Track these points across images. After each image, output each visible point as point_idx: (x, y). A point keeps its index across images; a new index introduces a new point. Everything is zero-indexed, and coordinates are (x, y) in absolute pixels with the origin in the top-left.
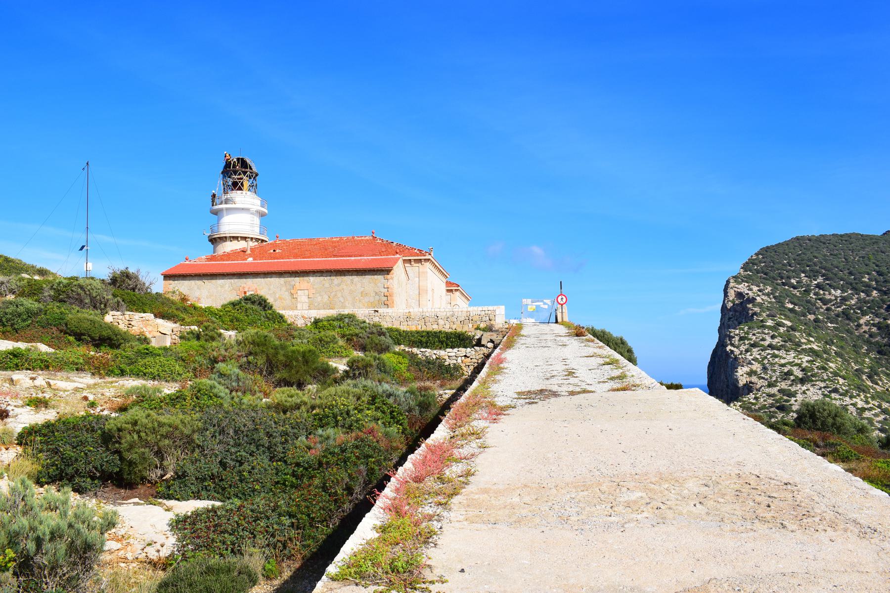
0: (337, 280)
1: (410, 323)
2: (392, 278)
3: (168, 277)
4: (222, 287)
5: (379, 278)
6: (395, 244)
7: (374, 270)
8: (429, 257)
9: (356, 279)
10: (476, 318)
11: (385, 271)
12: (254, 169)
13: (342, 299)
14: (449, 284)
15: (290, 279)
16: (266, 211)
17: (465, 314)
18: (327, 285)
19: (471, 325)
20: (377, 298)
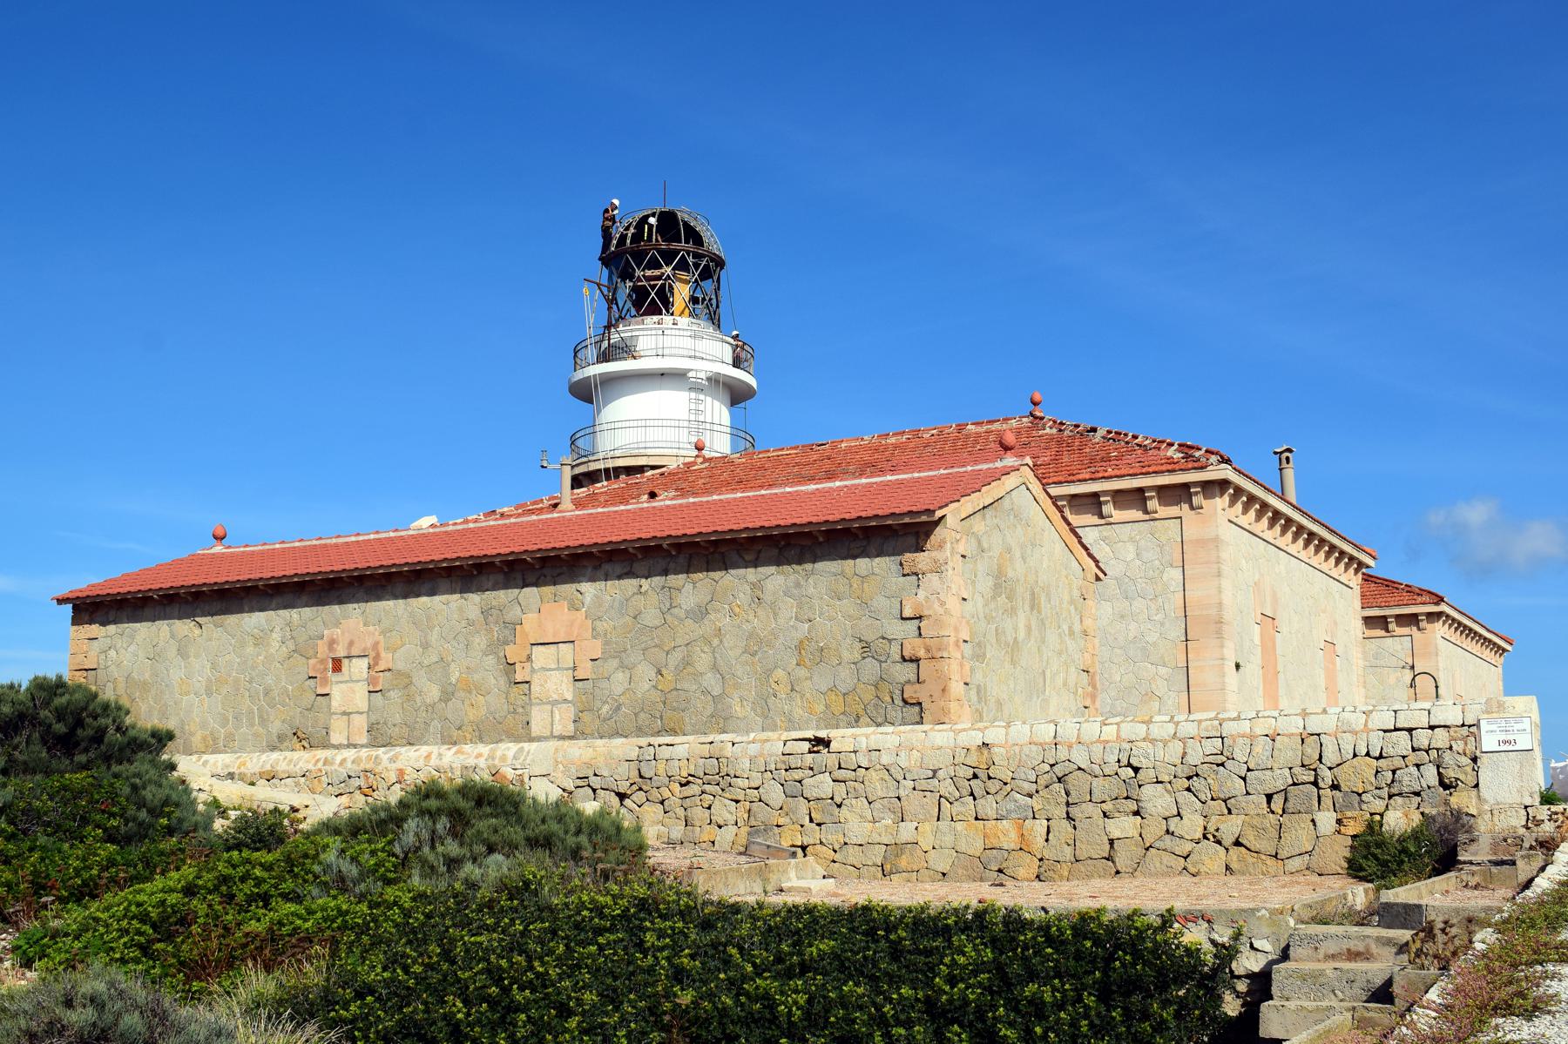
0: (691, 589)
1: (988, 806)
2: (938, 570)
3: (92, 609)
4: (259, 641)
5: (878, 568)
6: (1101, 432)
7: (847, 532)
8: (1226, 473)
9: (775, 579)
10: (1358, 775)
11: (903, 533)
12: (714, 243)
13: (711, 681)
14: (1376, 586)
15: (502, 596)
16: (753, 382)
17: (1289, 753)
18: (651, 617)
19: (1327, 820)
20: (871, 668)
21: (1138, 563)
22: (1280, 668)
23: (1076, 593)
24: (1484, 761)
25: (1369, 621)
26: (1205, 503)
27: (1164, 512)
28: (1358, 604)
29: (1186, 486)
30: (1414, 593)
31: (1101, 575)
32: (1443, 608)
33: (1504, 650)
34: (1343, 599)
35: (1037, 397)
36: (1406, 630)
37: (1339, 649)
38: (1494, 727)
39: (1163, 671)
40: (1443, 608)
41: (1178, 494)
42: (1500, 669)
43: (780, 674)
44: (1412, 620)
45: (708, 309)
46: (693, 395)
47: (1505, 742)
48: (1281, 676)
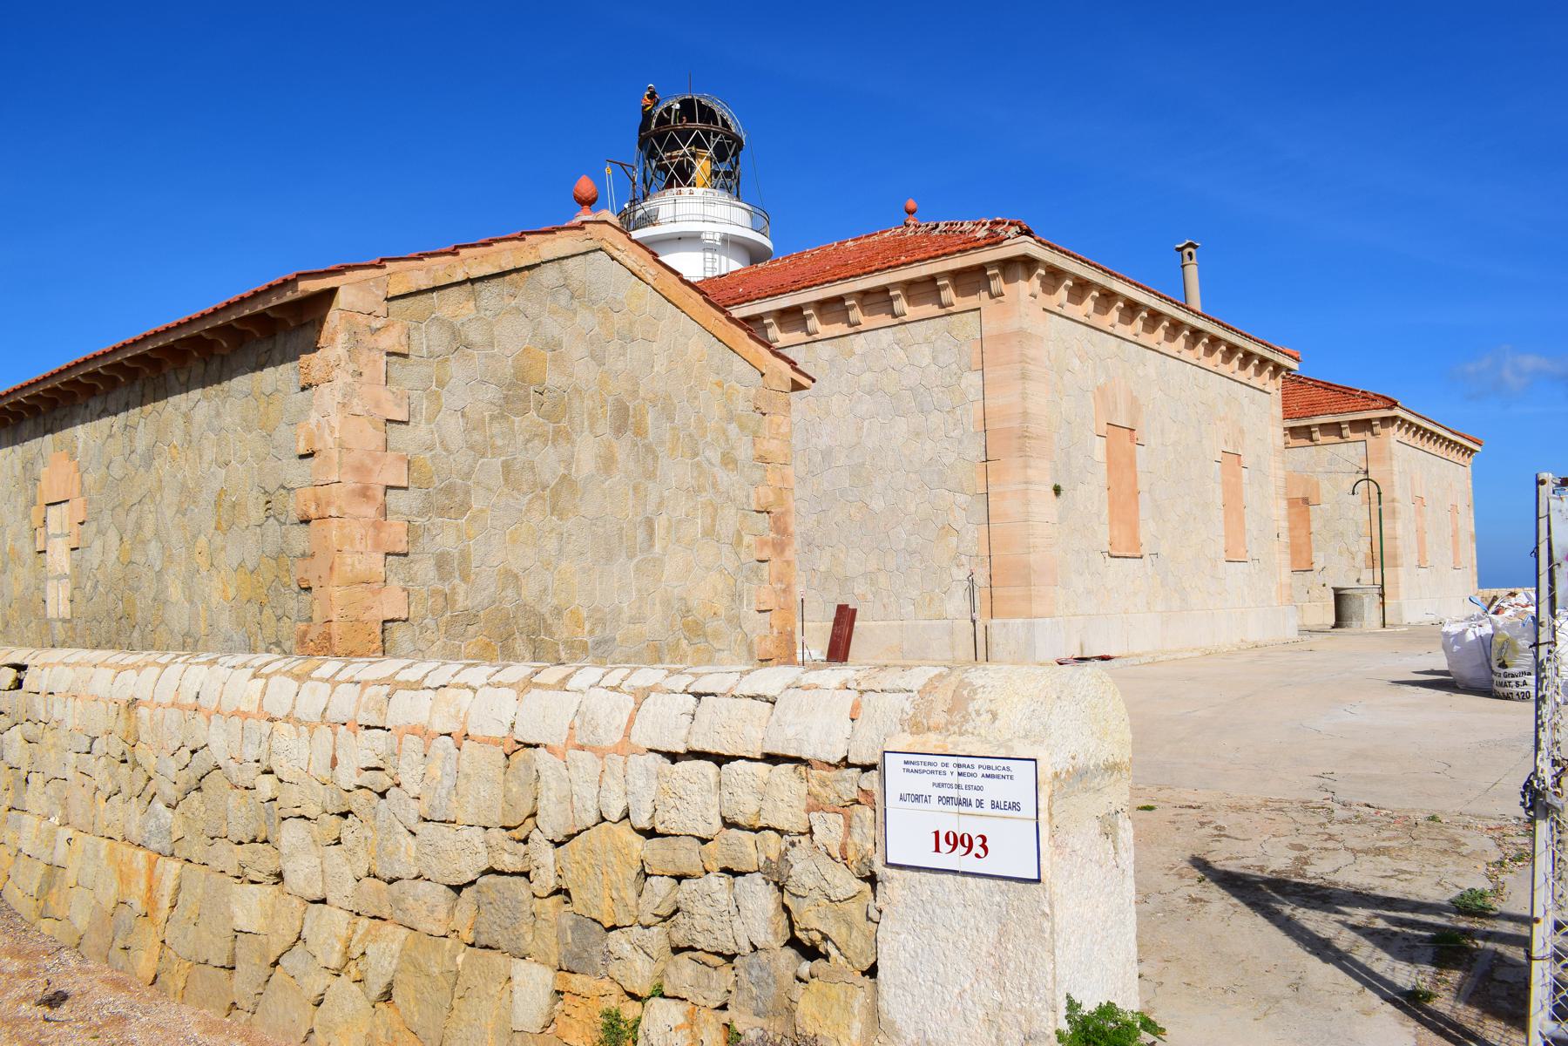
8: (1028, 247)
16: (768, 243)
21: (934, 368)
22: (1142, 485)
23: (741, 406)
24: (895, 887)
25: (1293, 432)
26: (1005, 288)
27: (961, 303)
28: (1278, 411)
29: (981, 268)
30: (1368, 398)
31: (804, 381)
32: (1397, 412)
33: (1472, 451)
34: (1259, 407)
35: (911, 204)
36: (1360, 436)
37: (1245, 461)
38: (922, 784)
39: (960, 498)
40: (1397, 412)
41: (972, 279)
42: (1469, 469)
43: (203, 540)
44: (1366, 425)
45: (728, 182)
46: (709, 255)
47: (956, 841)
48: (1144, 498)
